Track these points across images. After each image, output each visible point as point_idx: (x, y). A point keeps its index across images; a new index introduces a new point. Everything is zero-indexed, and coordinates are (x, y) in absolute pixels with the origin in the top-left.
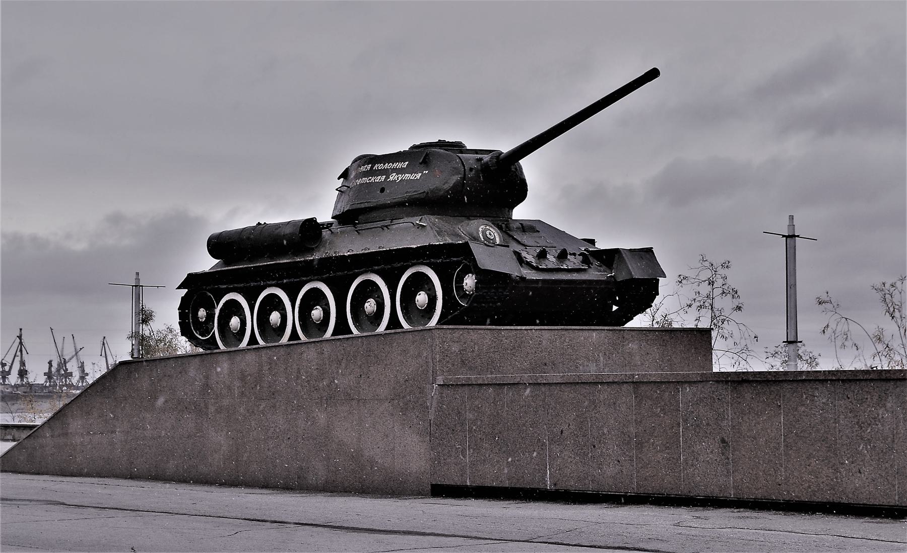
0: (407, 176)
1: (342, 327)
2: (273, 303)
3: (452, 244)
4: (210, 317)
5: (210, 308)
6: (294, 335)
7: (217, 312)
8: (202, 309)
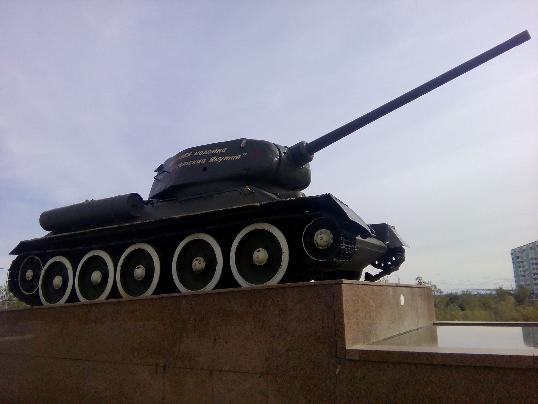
0: (227, 158)
1: (167, 284)
2: (97, 263)
3: (278, 203)
4: (36, 277)
5: (37, 269)
6: (73, 297)
7: (43, 272)
8: (30, 270)
